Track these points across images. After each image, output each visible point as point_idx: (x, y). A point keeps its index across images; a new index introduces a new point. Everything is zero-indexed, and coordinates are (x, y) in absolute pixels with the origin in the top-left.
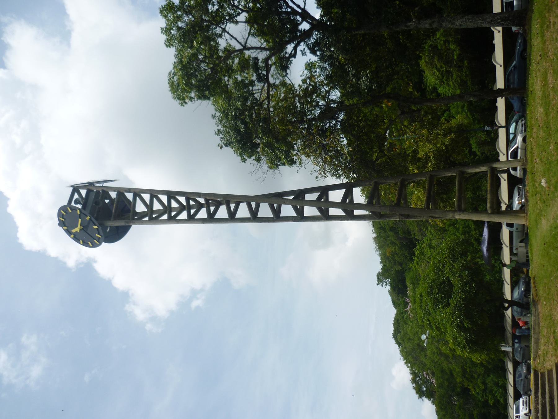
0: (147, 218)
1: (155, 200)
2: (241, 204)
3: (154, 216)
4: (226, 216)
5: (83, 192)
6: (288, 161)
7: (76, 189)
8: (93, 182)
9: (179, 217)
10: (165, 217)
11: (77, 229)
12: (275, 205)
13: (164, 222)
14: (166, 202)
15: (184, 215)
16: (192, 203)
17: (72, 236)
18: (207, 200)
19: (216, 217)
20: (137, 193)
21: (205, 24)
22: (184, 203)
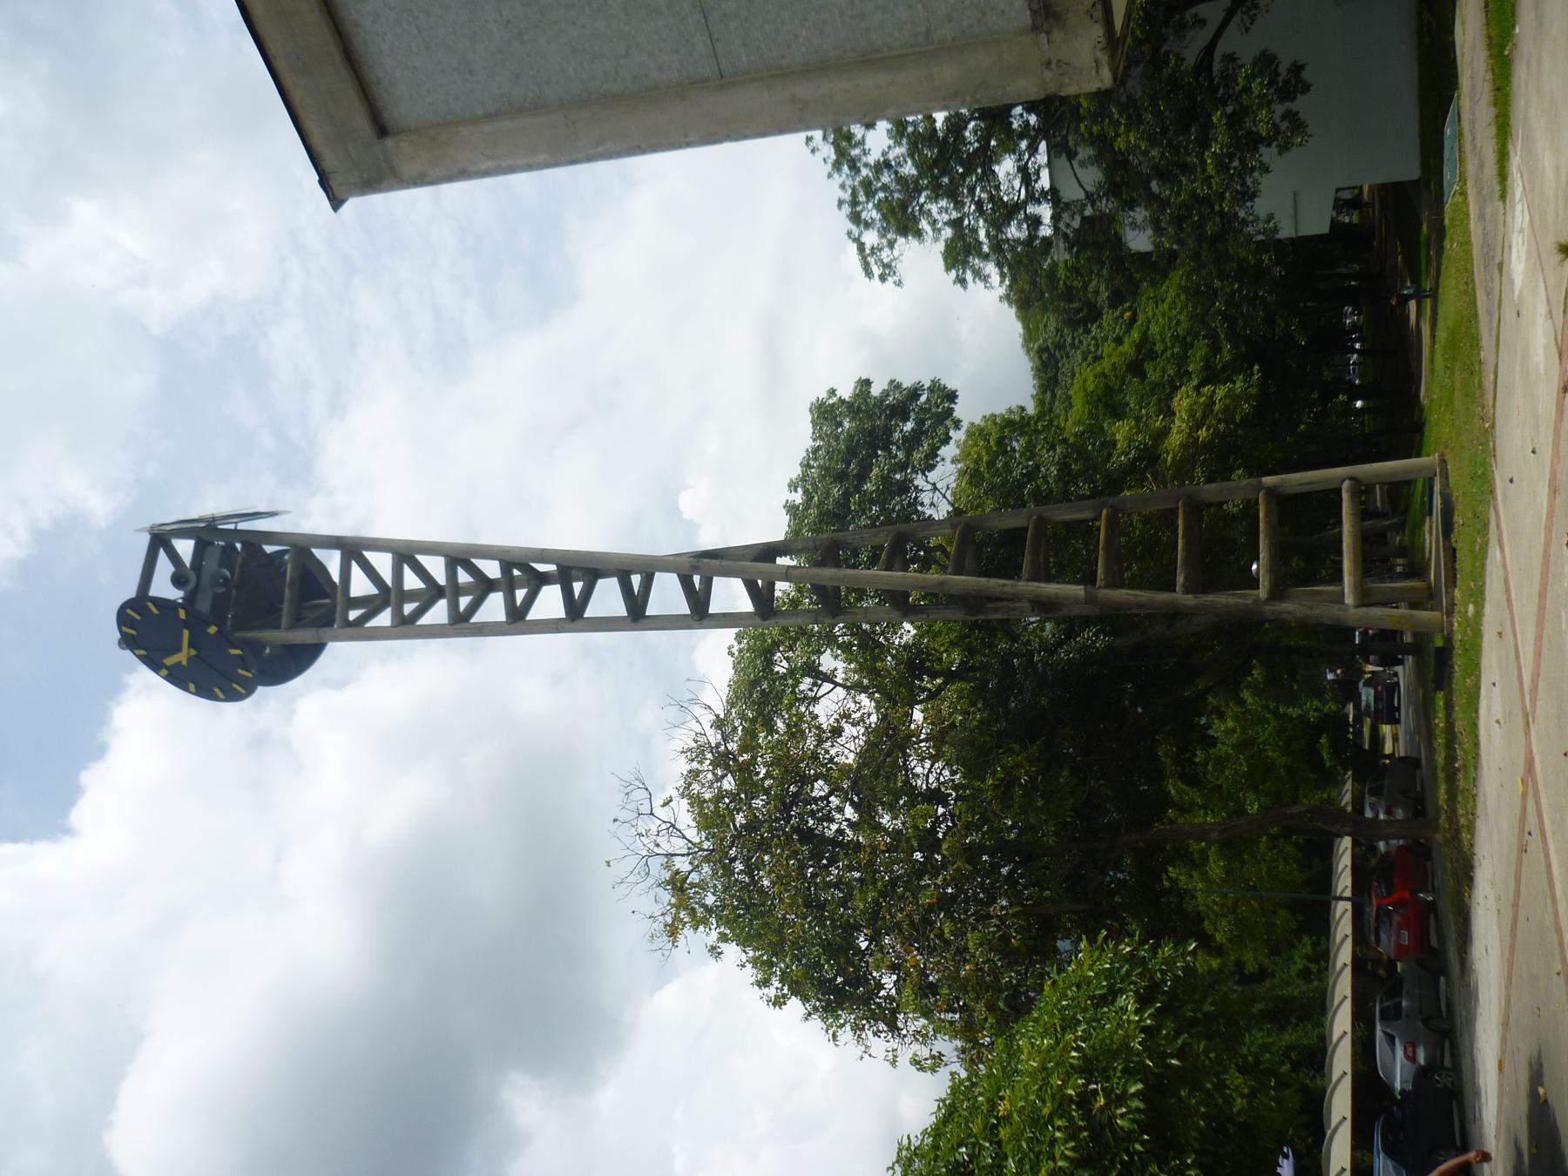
1: (354, 566)
2: (600, 582)
5: (185, 548)
7: (160, 540)
8: (214, 519)
9: (425, 620)
10: (384, 619)
11: (182, 657)
12: (696, 579)
13: (434, 632)
14: (387, 576)
15: (438, 613)
16: (464, 577)
17: (164, 672)
18: (506, 567)
20: (353, 550)
21: (1382, 816)
22: (441, 578)
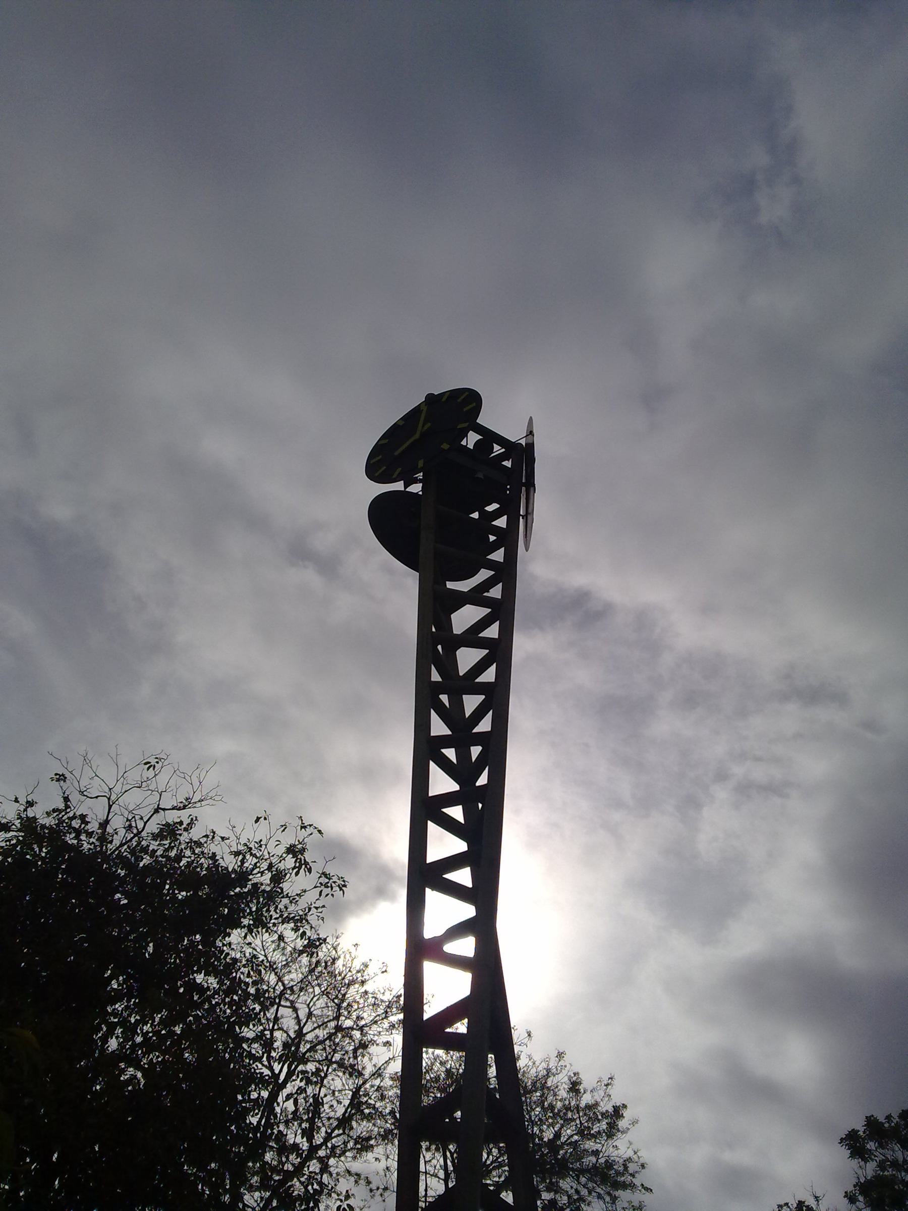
0: (435, 677)
3: (444, 698)
4: (433, 855)
6: (552, 1173)
19: (431, 826)
